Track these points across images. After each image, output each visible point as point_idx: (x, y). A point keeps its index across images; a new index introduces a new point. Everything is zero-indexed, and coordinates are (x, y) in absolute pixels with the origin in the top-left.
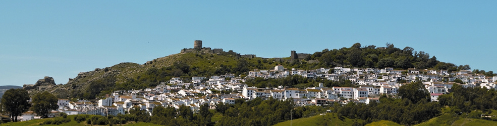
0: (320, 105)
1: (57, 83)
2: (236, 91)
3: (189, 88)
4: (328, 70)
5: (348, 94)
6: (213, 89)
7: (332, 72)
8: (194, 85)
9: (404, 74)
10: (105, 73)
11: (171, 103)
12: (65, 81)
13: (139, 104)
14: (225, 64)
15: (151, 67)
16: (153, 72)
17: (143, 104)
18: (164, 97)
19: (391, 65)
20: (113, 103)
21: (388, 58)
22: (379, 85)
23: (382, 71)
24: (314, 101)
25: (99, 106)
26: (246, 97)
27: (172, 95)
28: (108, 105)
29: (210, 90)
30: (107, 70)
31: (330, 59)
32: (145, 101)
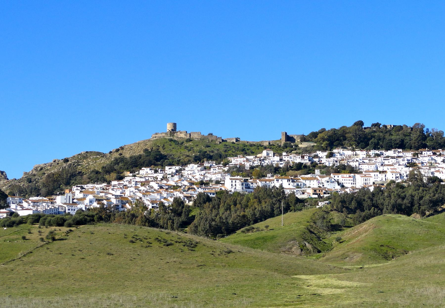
0: (316, 196)
1: (10, 177)
2: (218, 182)
3: (162, 180)
4: (326, 153)
5: (349, 182)
6: (190, 180)
7: (331, 155)
8: (168, 176)
9: (416, 155)
10: (65, 165)
11: (141, 198)
12: (19, 175)
13: (102, 200)
14: (205, 149)
15: (117, 155)
16: (120, 160)
17: (108, 199)
18: (132, 191)
19: (402, 145)
20: (73, 199)
21: (395, 137)
22: (385, 168)
23: (390, 153)
24: (310, 191)
25: (57, 204)
26: (229, 189)
27: (142, 188)
28: (68, 202)
29: (187, 181)
30: (66, 160)
31: (334, 140)
32: (110, 196)
